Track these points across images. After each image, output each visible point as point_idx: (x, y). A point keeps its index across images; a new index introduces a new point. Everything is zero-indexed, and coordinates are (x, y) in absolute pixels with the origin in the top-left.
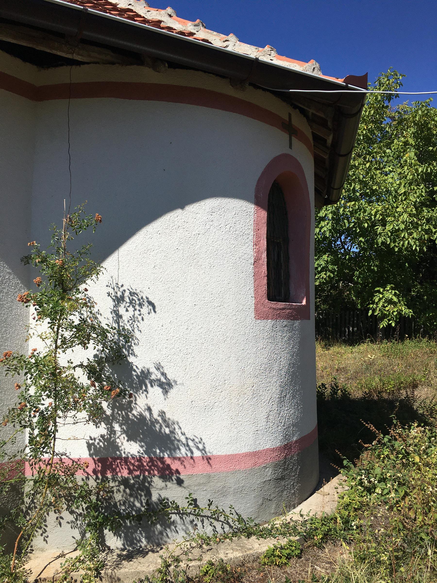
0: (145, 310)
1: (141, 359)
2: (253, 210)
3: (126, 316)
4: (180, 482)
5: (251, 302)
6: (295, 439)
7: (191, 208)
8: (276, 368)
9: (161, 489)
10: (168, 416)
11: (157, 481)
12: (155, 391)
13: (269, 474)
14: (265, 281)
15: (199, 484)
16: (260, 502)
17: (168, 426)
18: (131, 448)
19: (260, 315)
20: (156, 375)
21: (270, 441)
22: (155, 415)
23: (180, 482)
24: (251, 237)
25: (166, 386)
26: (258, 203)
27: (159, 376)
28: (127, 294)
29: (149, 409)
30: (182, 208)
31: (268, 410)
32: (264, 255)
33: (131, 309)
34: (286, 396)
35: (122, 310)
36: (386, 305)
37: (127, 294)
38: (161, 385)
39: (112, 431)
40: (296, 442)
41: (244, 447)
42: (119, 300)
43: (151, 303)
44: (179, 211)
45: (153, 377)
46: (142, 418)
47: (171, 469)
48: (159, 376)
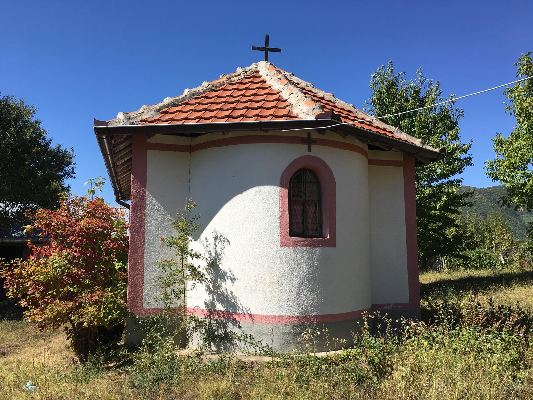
0: (226, 243)
1: (224, 266)
2: (279, 190)
3: (219, 246)
4: (240, 327)
5: (278, 238)
6: (313, 314)
7: (246, 193)
8: (296, 273)
9: (231, 328)
10: (234, 294)
11: (230, 324)
12: (229, 281)
13: (289, 328)
14: (288, 226)
15: (248, 327)
16: (283, 342)
17: (234, 299)
18: (220, 307)
19: (283, 244)
20: (229, 274)
21: (291, 311)
22: (229, 293)
23: (240, 327)
24: (278, 204)
25: (233, 280)
26: (282, 185)
27: (231, 275)
28: (219, 236)
29: (226, 290)
30: (241, 193)
31: (289, 295)
32: (287, 213)
33: (220, 243)
34: (305, 289)
35: (217, 244)
36: (102, 203)
37: (219, 236)
38: (231, 279)
39: (213, 299)
40: (315, 316)
41: (274, 311)
42: (216, 238)
43: (228, 241)
44: (240, 195)
45: (228, 275)
46: (223, 294)
47: (236, 321)
48: (231, 275)
